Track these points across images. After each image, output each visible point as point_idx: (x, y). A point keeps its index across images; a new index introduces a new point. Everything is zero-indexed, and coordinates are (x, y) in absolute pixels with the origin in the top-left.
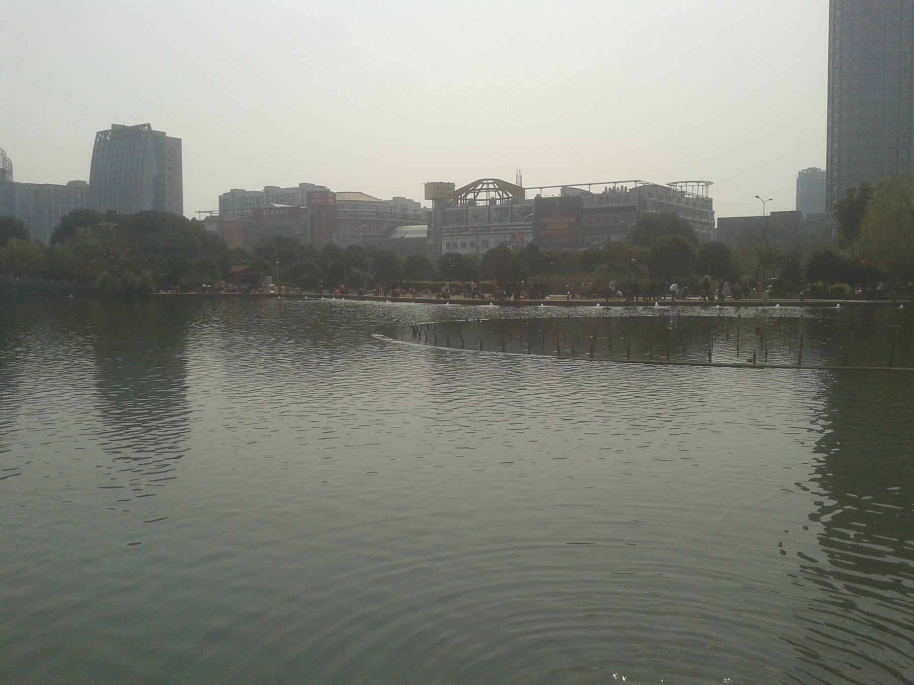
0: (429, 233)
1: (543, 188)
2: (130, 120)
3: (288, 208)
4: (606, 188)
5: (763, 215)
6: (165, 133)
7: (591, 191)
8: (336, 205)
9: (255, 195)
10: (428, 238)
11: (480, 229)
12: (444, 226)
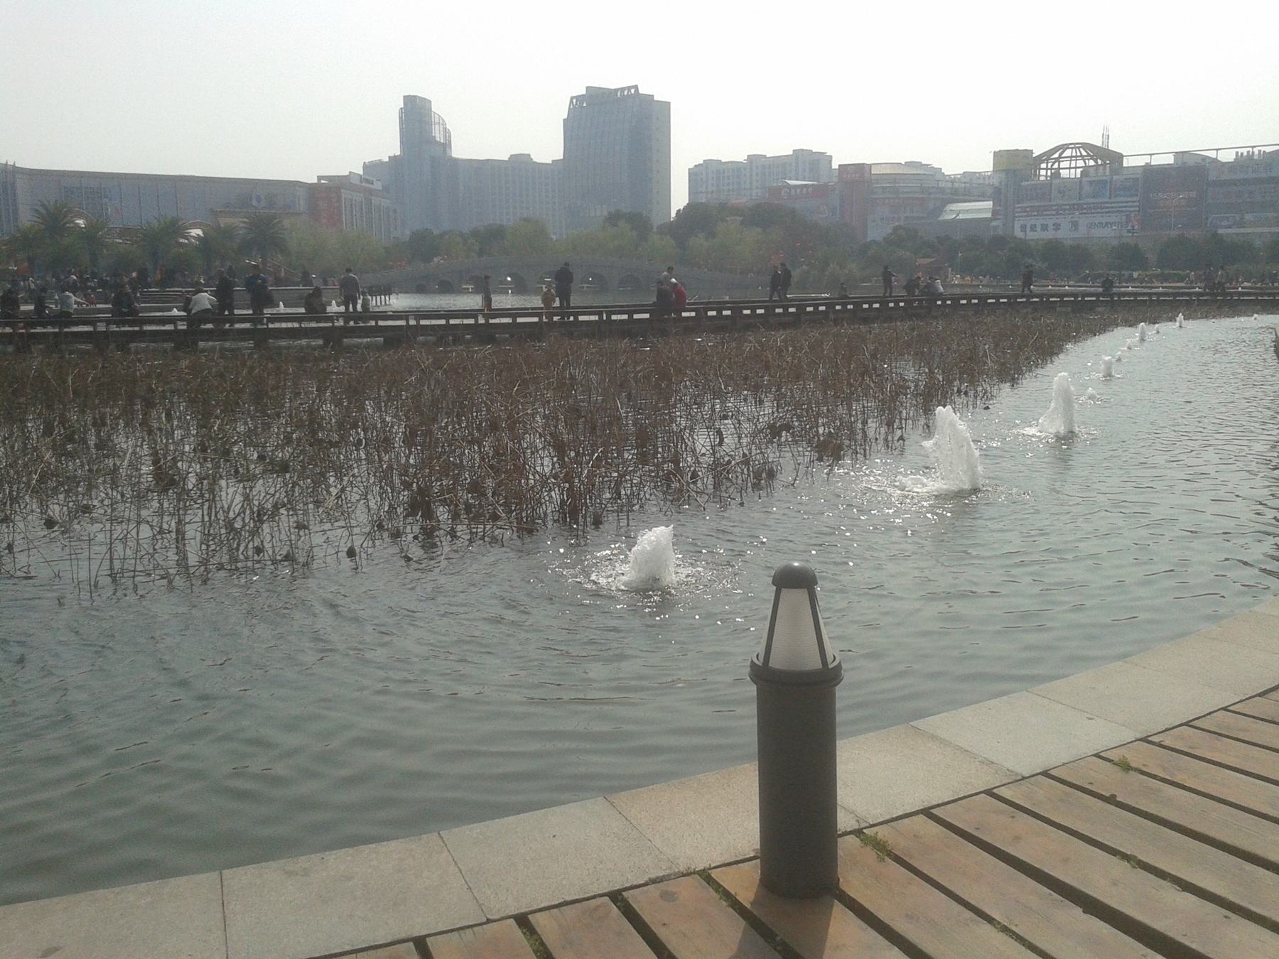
0: (994, 212)
1: (1154, 154)
2: (612, 80)
3: (813, 185)
4: (1237, 153)
5: (226, 872)
6: (653, 96)
7: (1218, 159)
8: (871, 180)
9: (735, 168)
10: (993, 218)
11: (1068, 207)
12: (1018, 203)
